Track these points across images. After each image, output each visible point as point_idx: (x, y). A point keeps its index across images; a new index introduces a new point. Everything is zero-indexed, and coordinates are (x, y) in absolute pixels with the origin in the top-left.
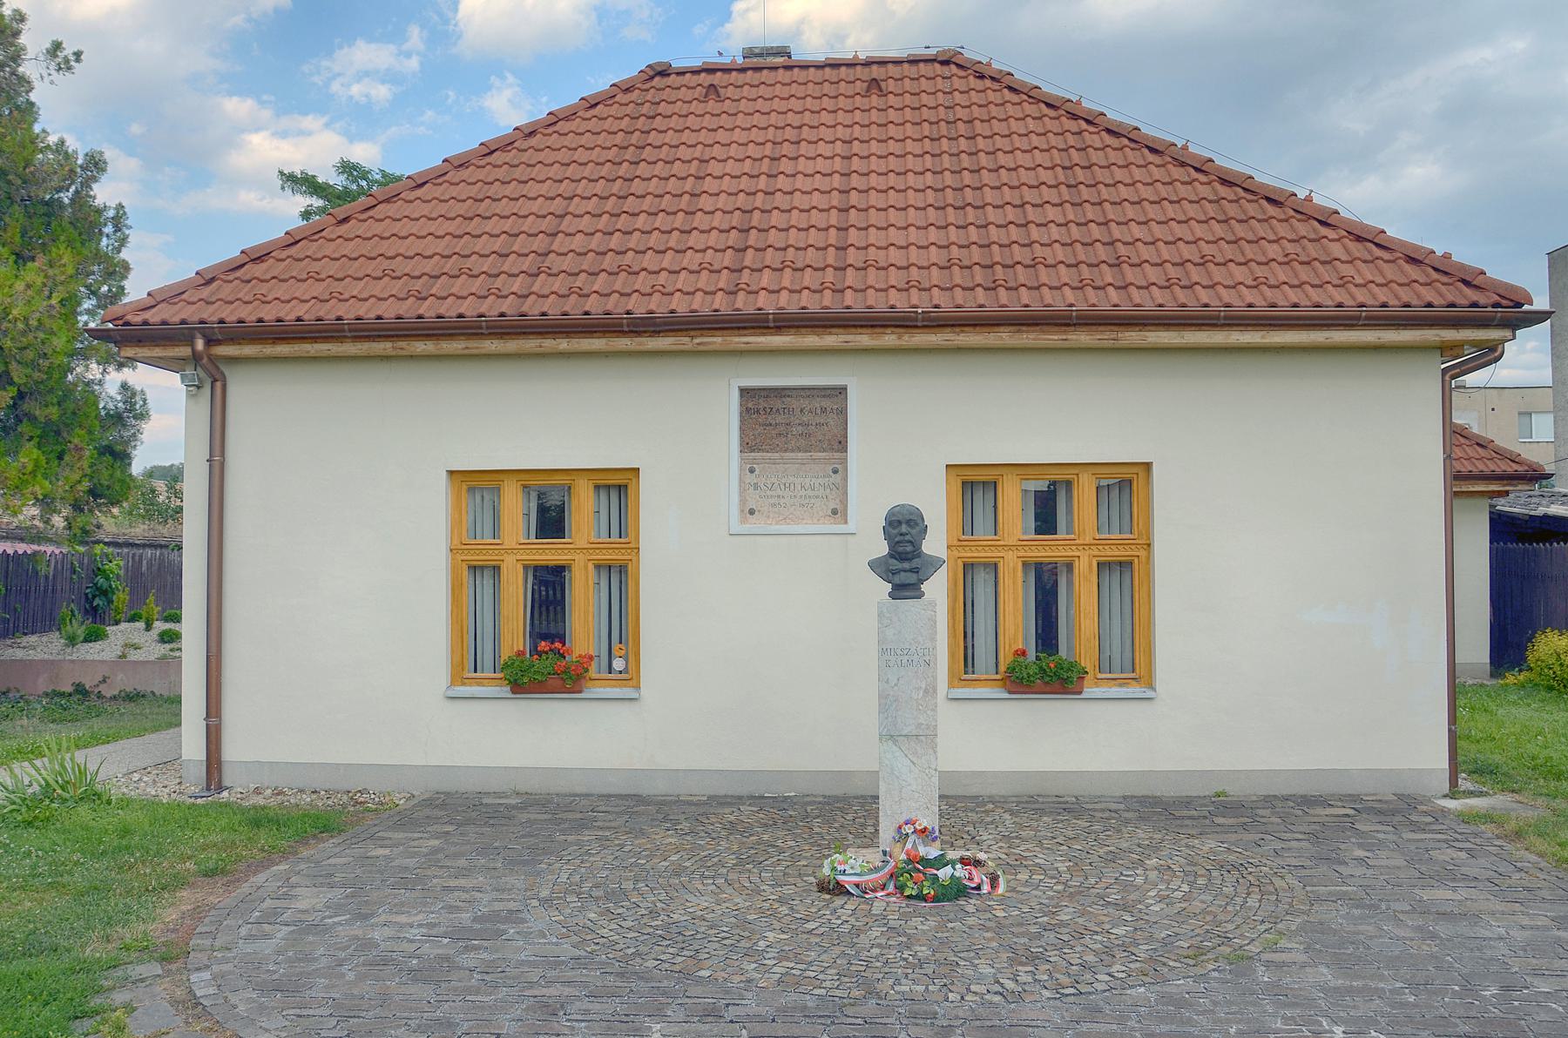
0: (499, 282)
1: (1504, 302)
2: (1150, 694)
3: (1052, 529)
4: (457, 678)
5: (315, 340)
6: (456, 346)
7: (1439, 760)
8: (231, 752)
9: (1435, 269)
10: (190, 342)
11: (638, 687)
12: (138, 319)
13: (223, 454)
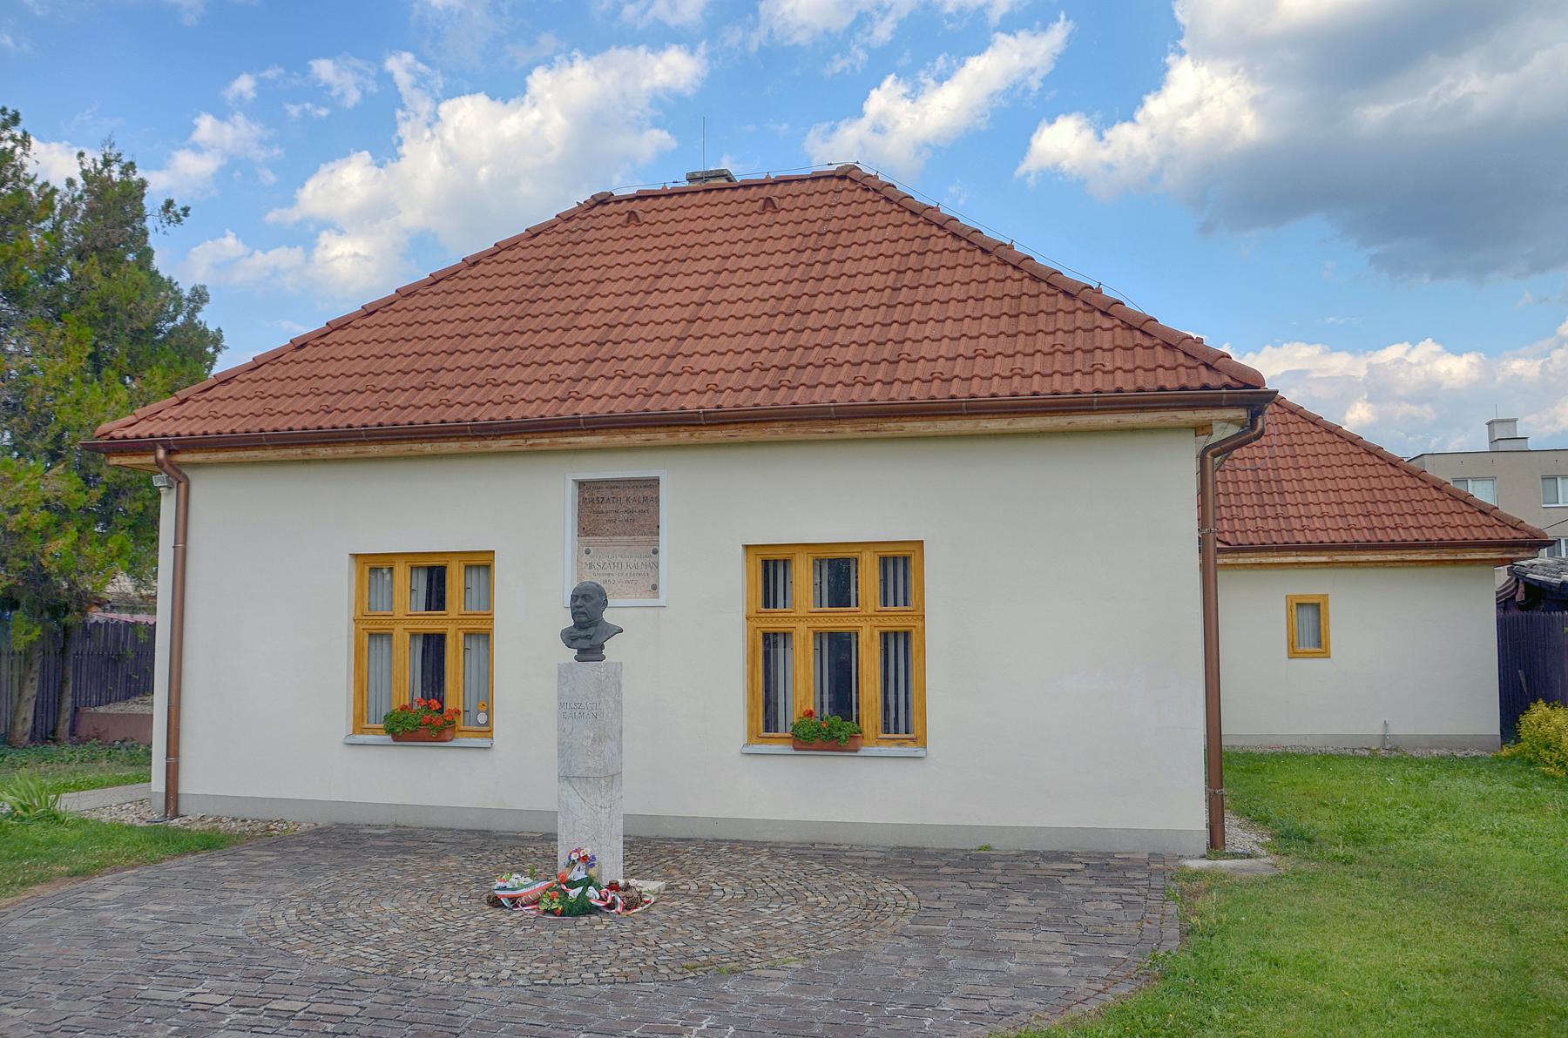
0: (579, 386)
1: (1234, 383)
2: (921, 753)
3: (441, 605)
4: (753, 737)
5: (245, 448)
6: (348, 451)
7: (1195, 818)
8: (186, 786)
9: (1186, 354)
10: (154, 451)
11: (924, 746)
12: (120, 434)
13: (185, 541)
